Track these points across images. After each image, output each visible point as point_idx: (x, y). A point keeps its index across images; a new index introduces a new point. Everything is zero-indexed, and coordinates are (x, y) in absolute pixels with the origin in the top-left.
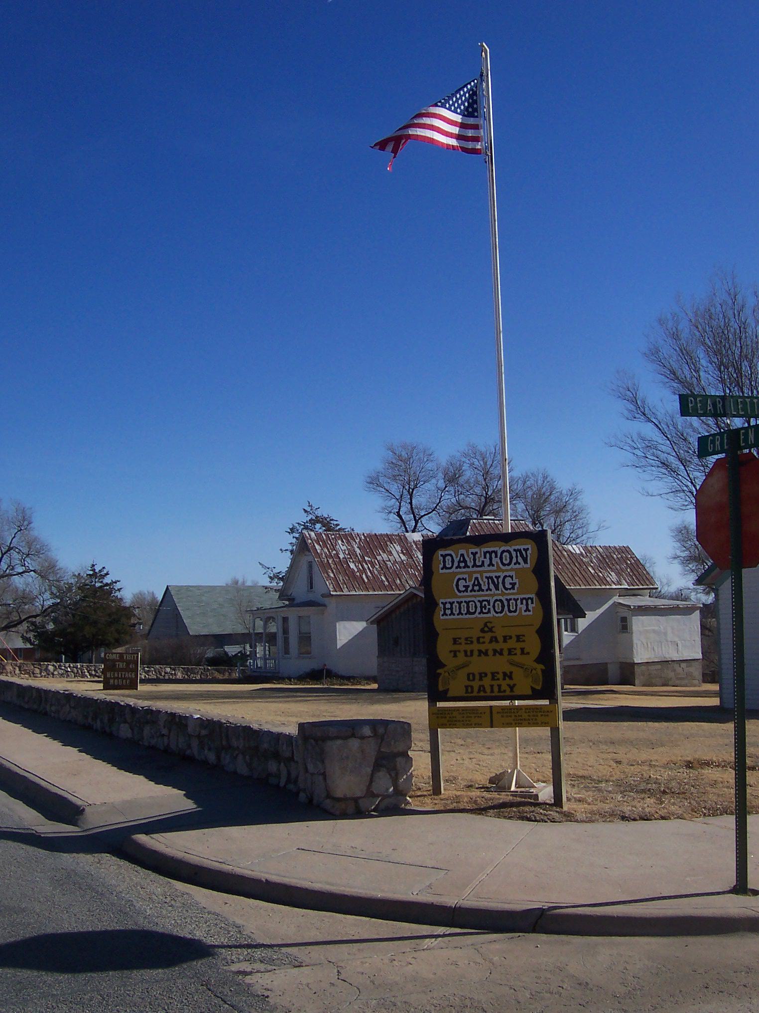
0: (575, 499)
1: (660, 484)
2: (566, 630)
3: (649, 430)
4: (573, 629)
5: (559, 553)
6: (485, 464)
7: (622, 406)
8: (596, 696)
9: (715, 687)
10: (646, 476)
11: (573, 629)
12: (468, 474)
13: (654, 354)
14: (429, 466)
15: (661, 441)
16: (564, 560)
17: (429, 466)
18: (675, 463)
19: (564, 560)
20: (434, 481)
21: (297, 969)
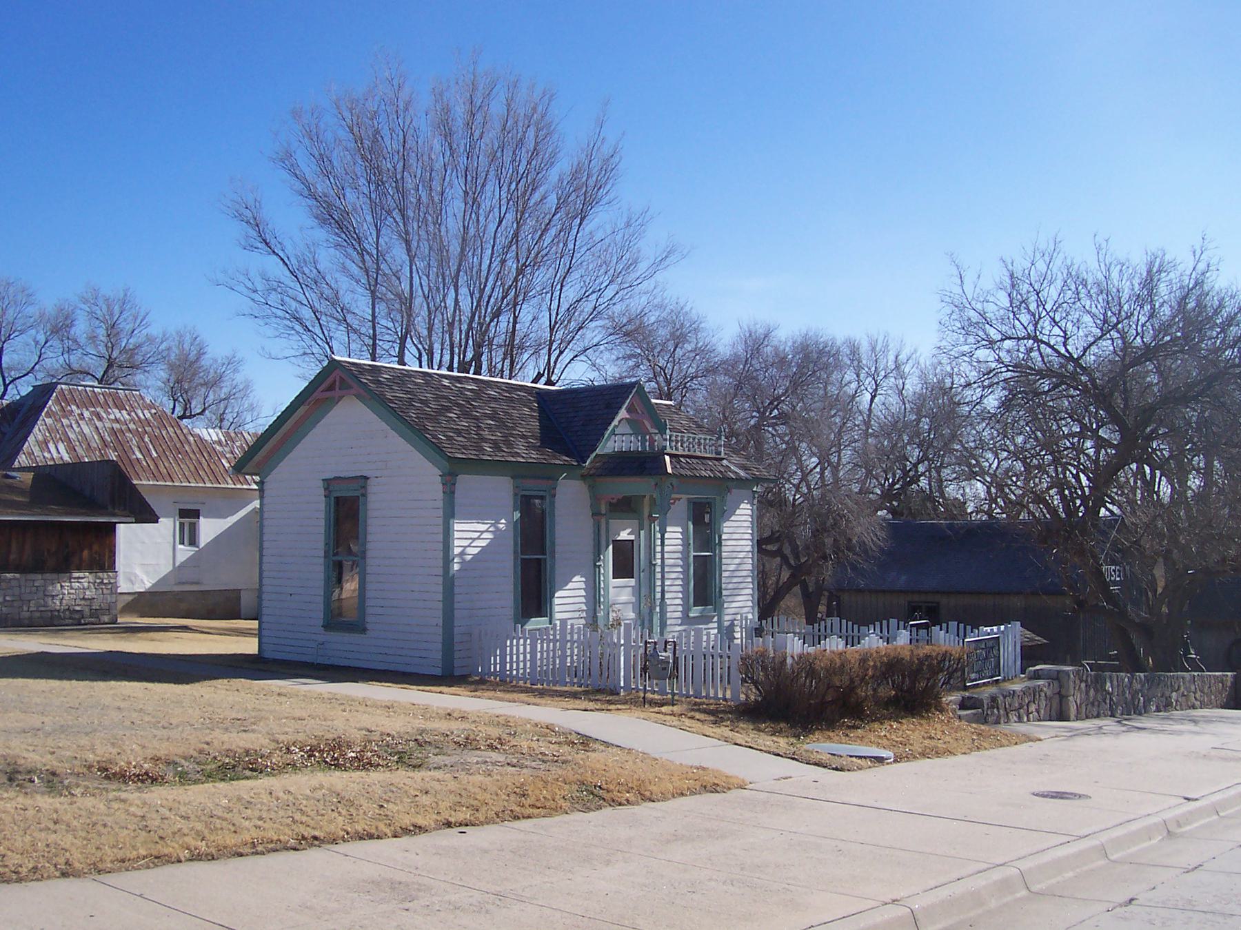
0: (235, 371)
1: (283, 342)
2: (182, 543)
3: (274, 267)
4: (193, 542)
5: (182, 438)
6: (112, 315)
7: (237, 230)
8: (145, 635)
9: (254, 624)
10: (269, 331)
11: (193, 542)
12: (81, 328)
13: (286, 160)
14: (30, 310)
15: (292, 284)
16: (187, 448)
17: (30, 310)
18: (306, 314)
19: (187, 448)
20: (33, 332)
21: (405, 841)
